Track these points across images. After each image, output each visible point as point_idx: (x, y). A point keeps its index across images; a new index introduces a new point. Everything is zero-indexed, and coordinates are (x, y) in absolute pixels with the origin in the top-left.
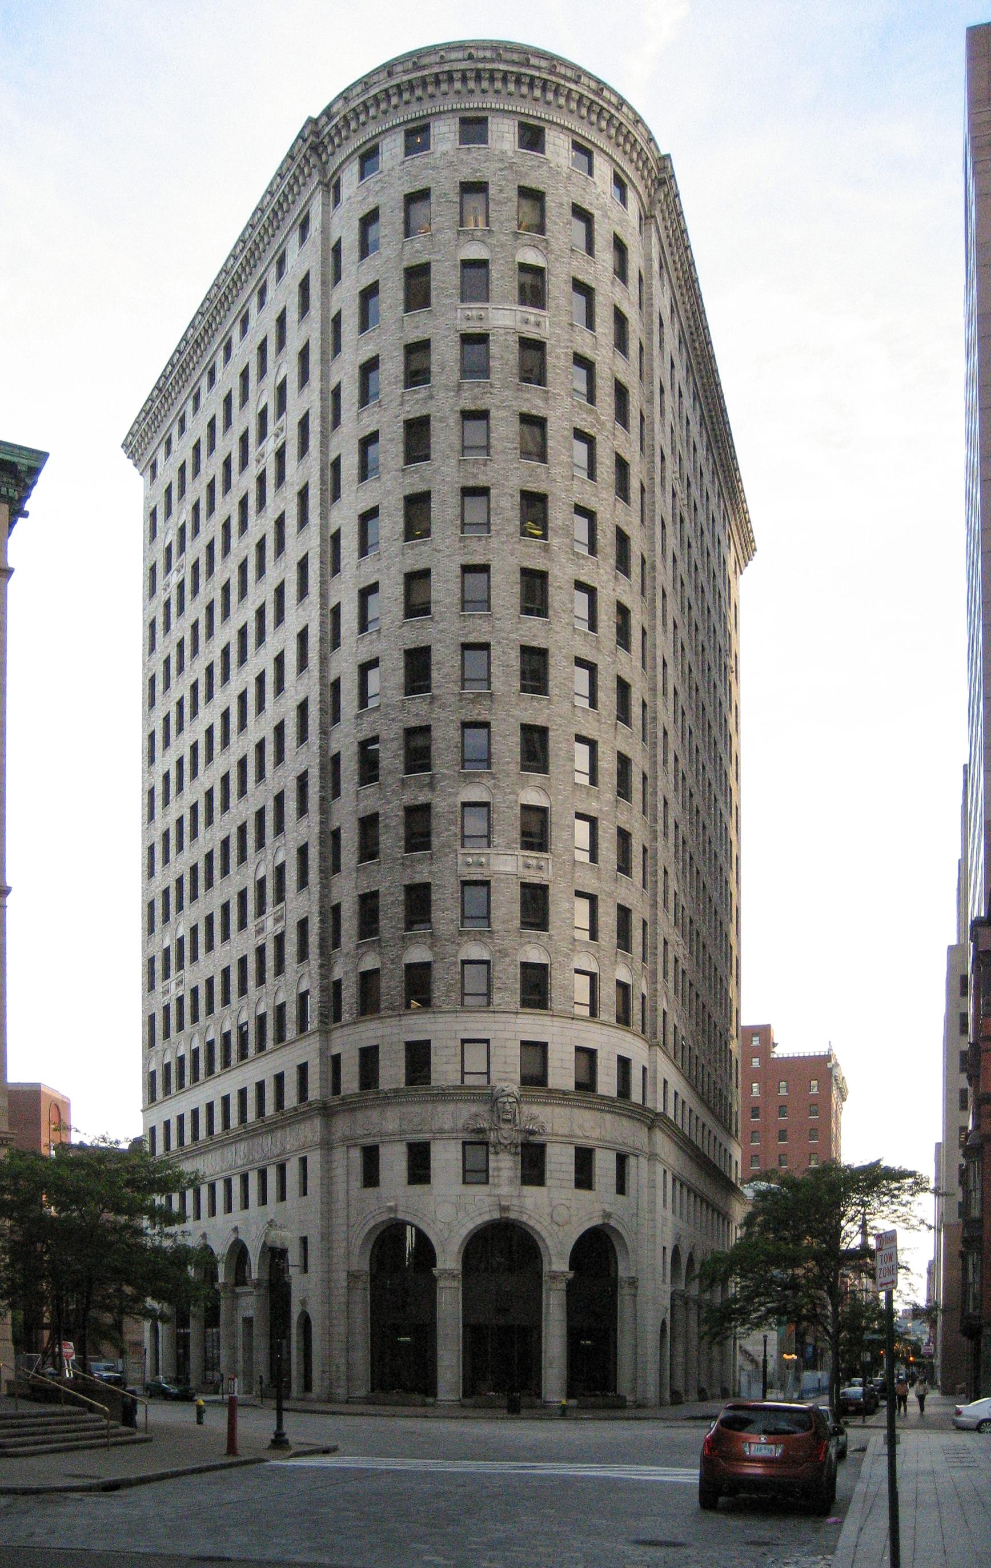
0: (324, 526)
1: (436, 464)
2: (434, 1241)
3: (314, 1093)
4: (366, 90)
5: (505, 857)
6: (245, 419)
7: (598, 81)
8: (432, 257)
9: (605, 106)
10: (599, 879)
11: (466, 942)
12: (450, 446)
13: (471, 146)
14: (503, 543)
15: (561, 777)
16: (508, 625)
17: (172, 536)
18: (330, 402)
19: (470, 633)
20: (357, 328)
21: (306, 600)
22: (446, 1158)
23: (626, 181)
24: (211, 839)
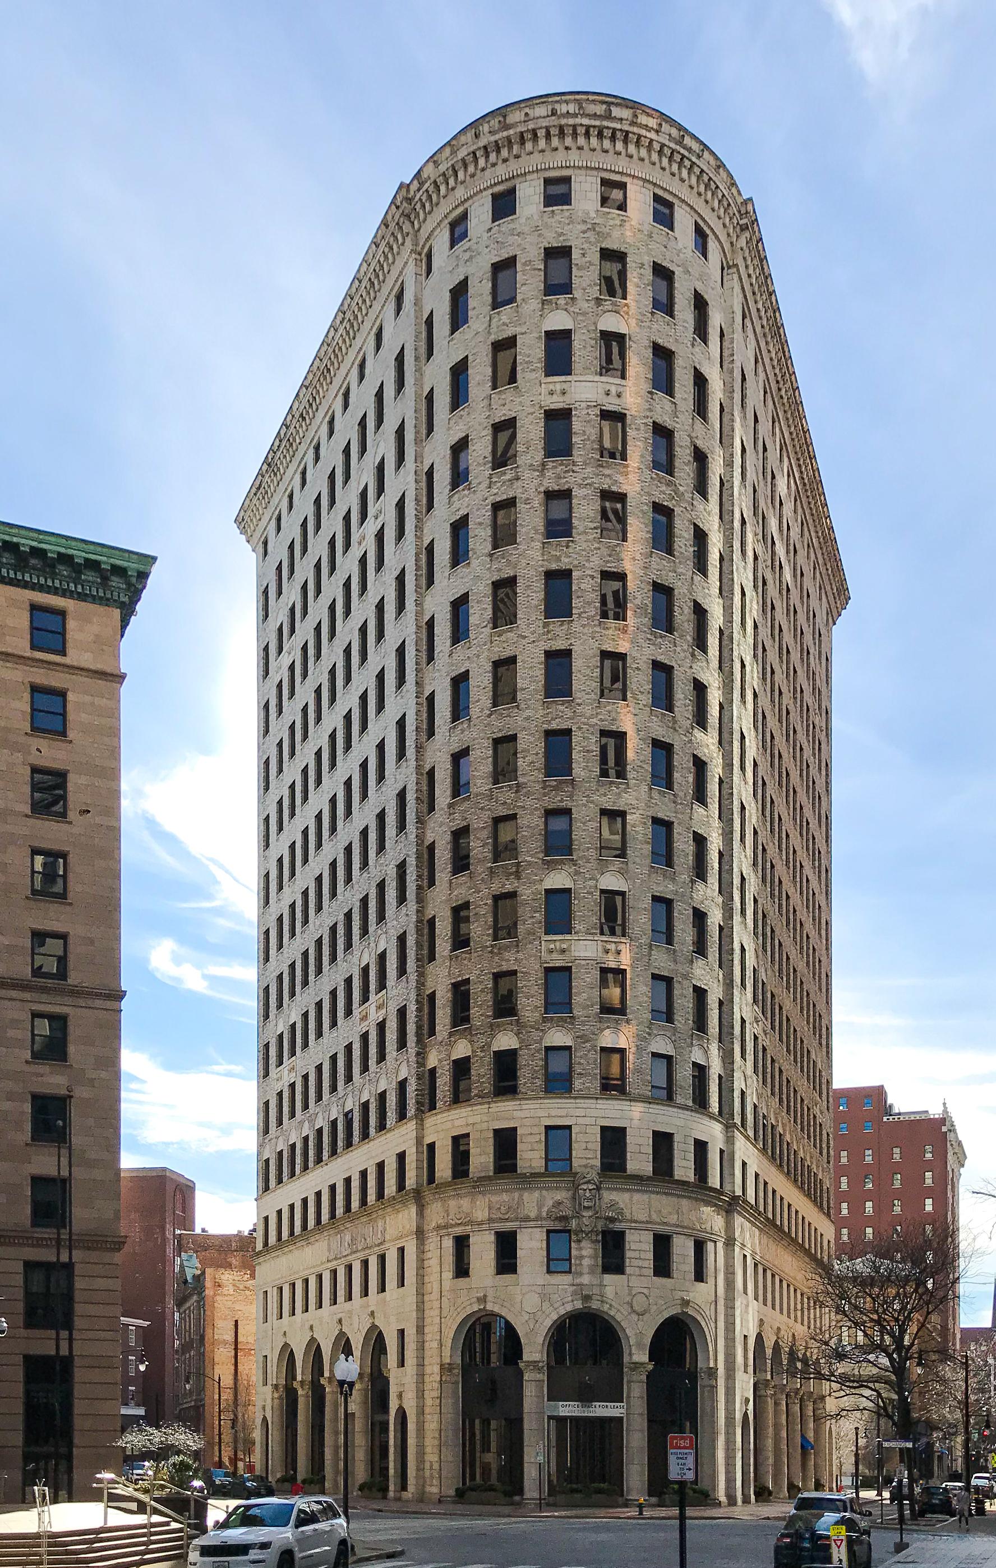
0: (419, 614)
1: (522, 547)
2: (521, 1332)
3: (410, 1182)
4: (454, 152)
5: (585, 942)
6: (348, 499)
7: (680, 128)
8: (518, 330)
9: (686, 153)
10: (675, 962)
11: (549, 1029)
12: (536, 532)
13: (555, 208)
14: (584, 626)
15: (637, 860)
16: (588, 710)
17: (283, 617)
18: (424, 484)
19: (553, 719)
20: (448, 407)
21: (404, 688)
22: (531, 1245)
23: (708, 232)
24: (320, 925)
